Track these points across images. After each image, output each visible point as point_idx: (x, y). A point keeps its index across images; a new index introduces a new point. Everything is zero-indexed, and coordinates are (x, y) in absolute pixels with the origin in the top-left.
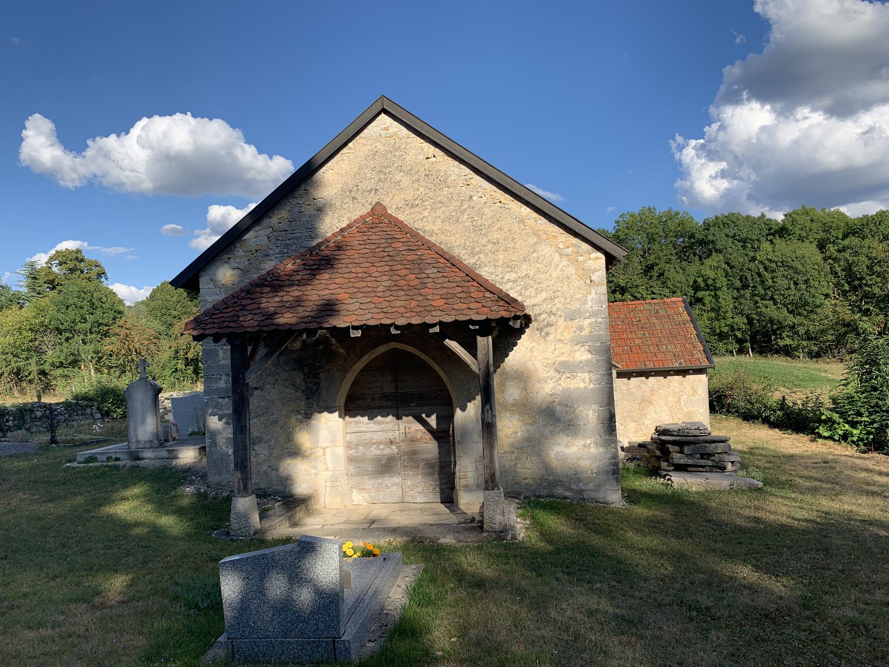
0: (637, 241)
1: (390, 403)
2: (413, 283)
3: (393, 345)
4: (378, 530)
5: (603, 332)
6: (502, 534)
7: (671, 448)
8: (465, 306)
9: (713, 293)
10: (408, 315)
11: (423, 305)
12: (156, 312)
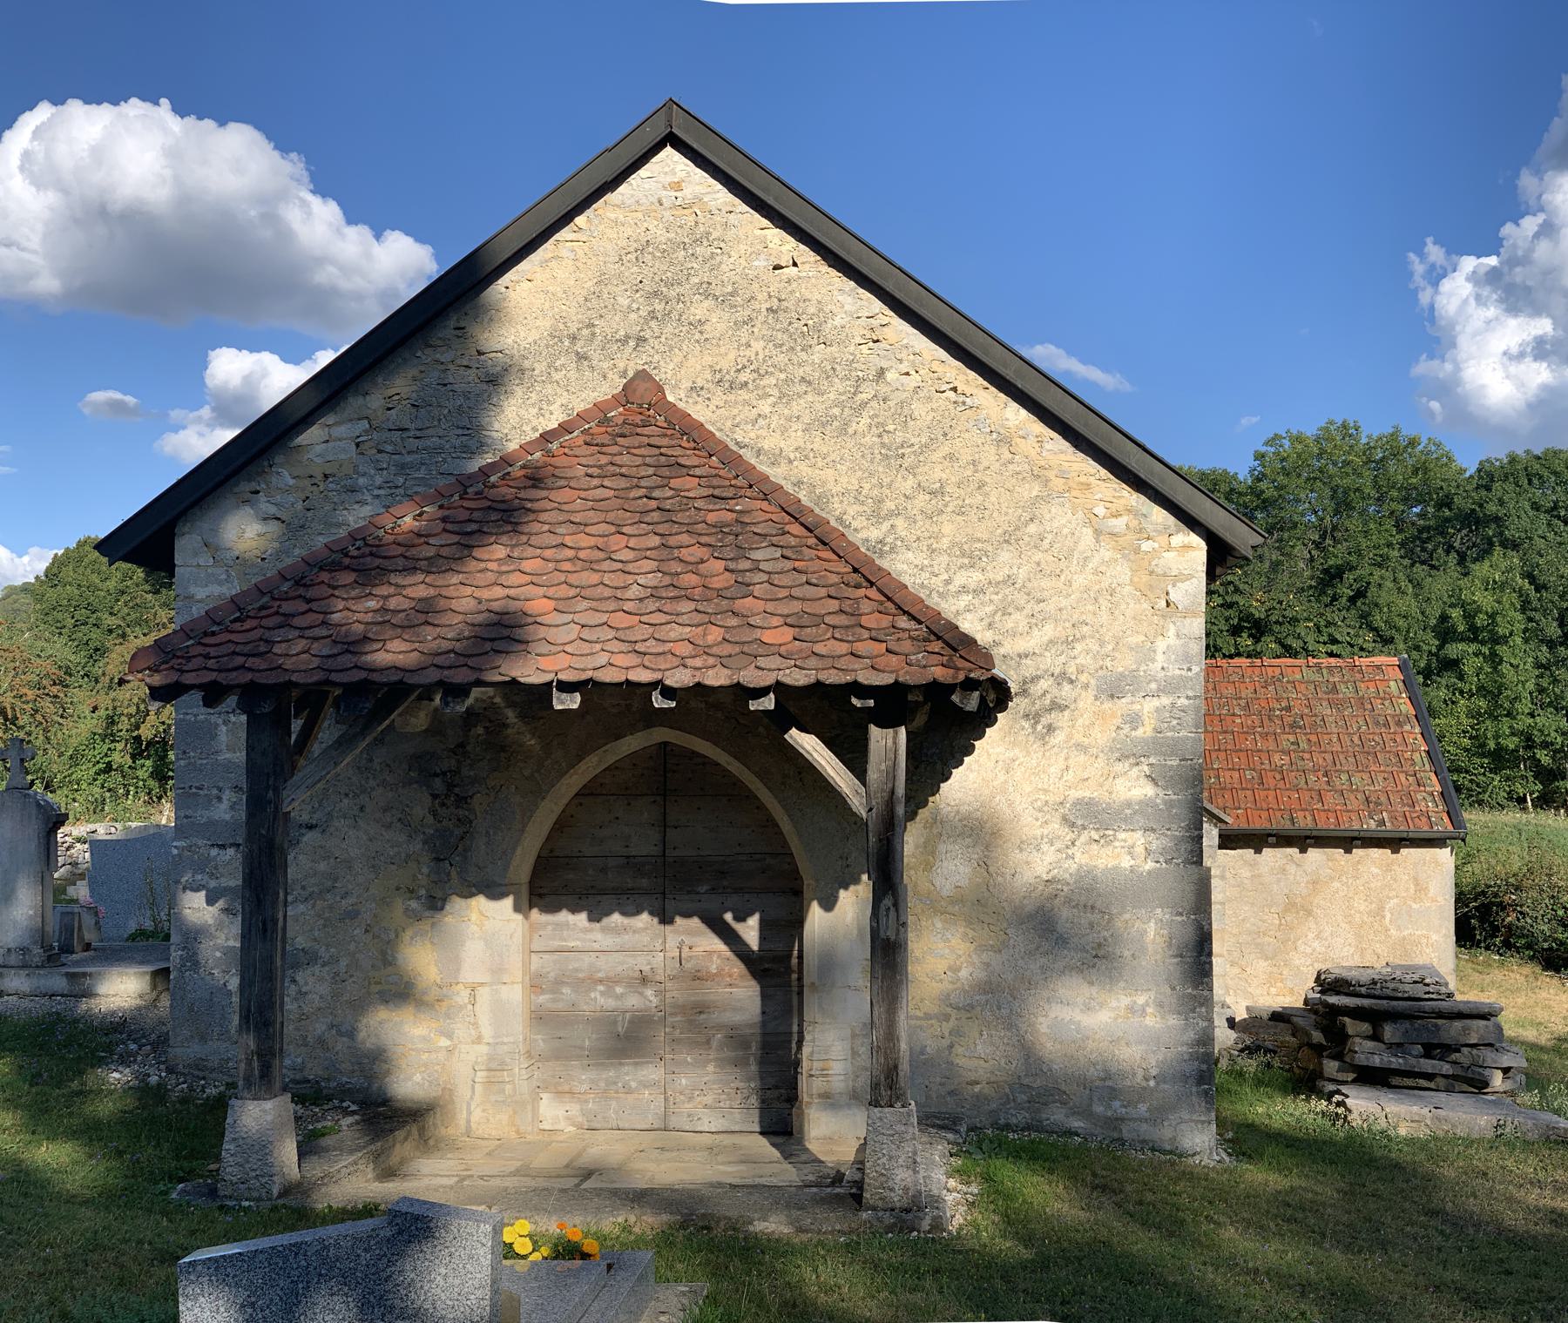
0: (1307, 505)
1: (644, 882)
2: (717, 583)
3: (661, 734)
4: (598, 1195)
5: (1187, 733)
6: (910, 1216)
7: (1351, 1026)
8: (843, 648)
9: (1485, 650)
10: (698, 662)
11: (737, 639)
12: (60, 616)
